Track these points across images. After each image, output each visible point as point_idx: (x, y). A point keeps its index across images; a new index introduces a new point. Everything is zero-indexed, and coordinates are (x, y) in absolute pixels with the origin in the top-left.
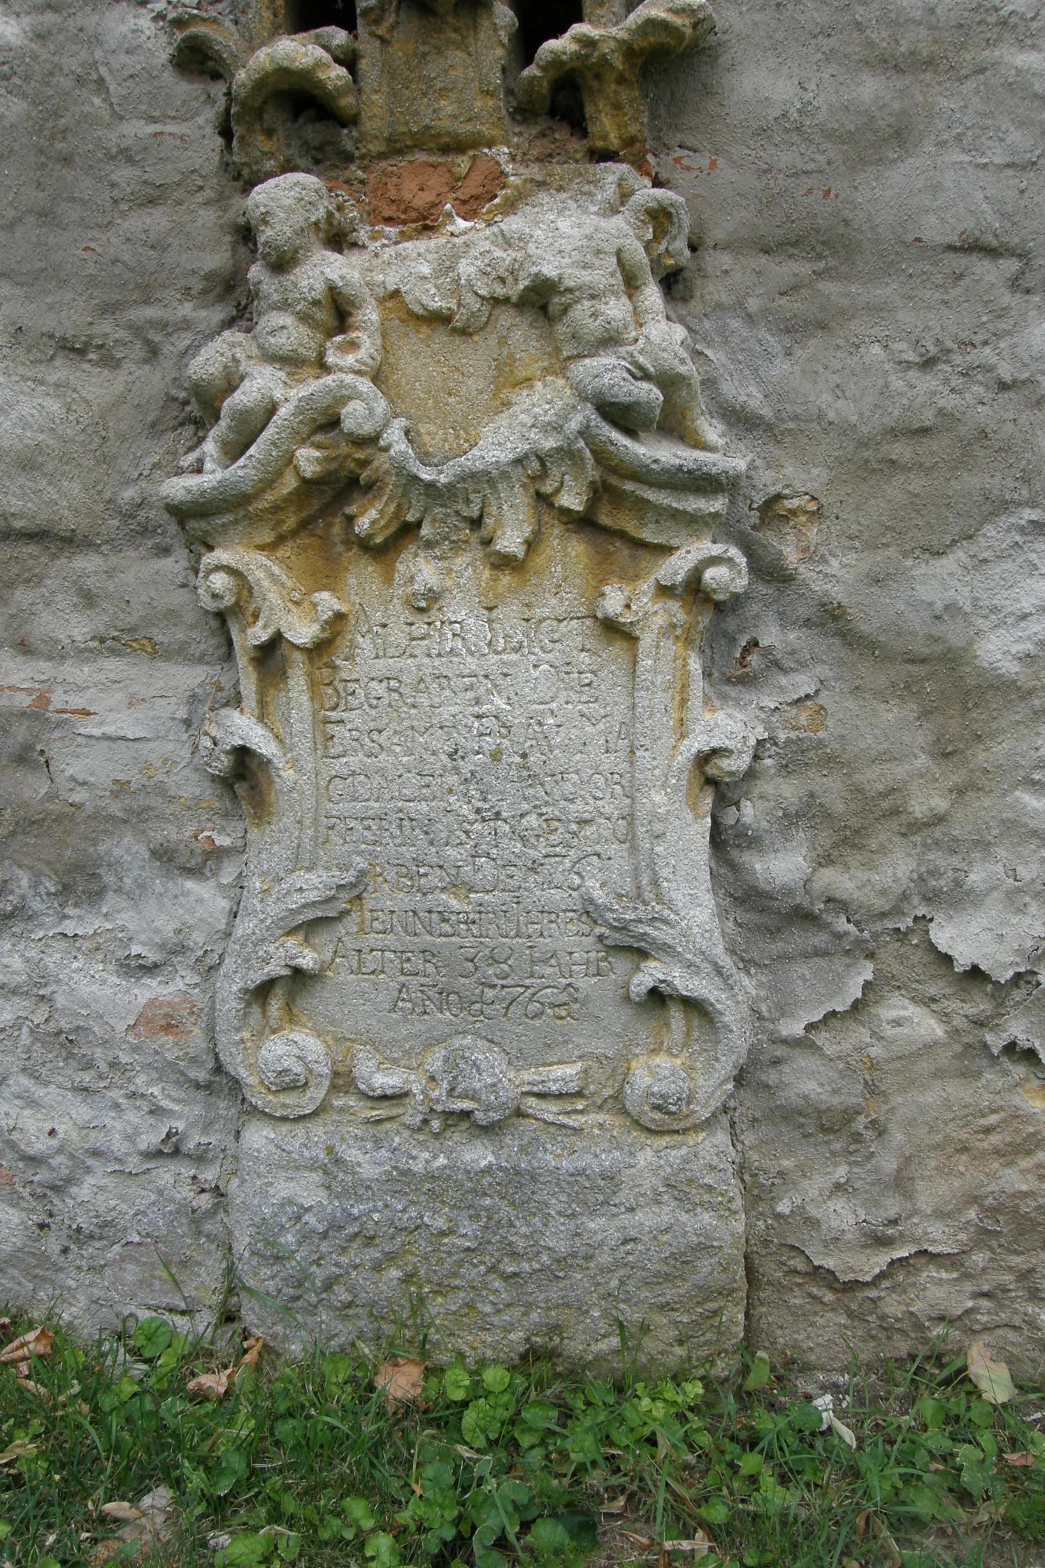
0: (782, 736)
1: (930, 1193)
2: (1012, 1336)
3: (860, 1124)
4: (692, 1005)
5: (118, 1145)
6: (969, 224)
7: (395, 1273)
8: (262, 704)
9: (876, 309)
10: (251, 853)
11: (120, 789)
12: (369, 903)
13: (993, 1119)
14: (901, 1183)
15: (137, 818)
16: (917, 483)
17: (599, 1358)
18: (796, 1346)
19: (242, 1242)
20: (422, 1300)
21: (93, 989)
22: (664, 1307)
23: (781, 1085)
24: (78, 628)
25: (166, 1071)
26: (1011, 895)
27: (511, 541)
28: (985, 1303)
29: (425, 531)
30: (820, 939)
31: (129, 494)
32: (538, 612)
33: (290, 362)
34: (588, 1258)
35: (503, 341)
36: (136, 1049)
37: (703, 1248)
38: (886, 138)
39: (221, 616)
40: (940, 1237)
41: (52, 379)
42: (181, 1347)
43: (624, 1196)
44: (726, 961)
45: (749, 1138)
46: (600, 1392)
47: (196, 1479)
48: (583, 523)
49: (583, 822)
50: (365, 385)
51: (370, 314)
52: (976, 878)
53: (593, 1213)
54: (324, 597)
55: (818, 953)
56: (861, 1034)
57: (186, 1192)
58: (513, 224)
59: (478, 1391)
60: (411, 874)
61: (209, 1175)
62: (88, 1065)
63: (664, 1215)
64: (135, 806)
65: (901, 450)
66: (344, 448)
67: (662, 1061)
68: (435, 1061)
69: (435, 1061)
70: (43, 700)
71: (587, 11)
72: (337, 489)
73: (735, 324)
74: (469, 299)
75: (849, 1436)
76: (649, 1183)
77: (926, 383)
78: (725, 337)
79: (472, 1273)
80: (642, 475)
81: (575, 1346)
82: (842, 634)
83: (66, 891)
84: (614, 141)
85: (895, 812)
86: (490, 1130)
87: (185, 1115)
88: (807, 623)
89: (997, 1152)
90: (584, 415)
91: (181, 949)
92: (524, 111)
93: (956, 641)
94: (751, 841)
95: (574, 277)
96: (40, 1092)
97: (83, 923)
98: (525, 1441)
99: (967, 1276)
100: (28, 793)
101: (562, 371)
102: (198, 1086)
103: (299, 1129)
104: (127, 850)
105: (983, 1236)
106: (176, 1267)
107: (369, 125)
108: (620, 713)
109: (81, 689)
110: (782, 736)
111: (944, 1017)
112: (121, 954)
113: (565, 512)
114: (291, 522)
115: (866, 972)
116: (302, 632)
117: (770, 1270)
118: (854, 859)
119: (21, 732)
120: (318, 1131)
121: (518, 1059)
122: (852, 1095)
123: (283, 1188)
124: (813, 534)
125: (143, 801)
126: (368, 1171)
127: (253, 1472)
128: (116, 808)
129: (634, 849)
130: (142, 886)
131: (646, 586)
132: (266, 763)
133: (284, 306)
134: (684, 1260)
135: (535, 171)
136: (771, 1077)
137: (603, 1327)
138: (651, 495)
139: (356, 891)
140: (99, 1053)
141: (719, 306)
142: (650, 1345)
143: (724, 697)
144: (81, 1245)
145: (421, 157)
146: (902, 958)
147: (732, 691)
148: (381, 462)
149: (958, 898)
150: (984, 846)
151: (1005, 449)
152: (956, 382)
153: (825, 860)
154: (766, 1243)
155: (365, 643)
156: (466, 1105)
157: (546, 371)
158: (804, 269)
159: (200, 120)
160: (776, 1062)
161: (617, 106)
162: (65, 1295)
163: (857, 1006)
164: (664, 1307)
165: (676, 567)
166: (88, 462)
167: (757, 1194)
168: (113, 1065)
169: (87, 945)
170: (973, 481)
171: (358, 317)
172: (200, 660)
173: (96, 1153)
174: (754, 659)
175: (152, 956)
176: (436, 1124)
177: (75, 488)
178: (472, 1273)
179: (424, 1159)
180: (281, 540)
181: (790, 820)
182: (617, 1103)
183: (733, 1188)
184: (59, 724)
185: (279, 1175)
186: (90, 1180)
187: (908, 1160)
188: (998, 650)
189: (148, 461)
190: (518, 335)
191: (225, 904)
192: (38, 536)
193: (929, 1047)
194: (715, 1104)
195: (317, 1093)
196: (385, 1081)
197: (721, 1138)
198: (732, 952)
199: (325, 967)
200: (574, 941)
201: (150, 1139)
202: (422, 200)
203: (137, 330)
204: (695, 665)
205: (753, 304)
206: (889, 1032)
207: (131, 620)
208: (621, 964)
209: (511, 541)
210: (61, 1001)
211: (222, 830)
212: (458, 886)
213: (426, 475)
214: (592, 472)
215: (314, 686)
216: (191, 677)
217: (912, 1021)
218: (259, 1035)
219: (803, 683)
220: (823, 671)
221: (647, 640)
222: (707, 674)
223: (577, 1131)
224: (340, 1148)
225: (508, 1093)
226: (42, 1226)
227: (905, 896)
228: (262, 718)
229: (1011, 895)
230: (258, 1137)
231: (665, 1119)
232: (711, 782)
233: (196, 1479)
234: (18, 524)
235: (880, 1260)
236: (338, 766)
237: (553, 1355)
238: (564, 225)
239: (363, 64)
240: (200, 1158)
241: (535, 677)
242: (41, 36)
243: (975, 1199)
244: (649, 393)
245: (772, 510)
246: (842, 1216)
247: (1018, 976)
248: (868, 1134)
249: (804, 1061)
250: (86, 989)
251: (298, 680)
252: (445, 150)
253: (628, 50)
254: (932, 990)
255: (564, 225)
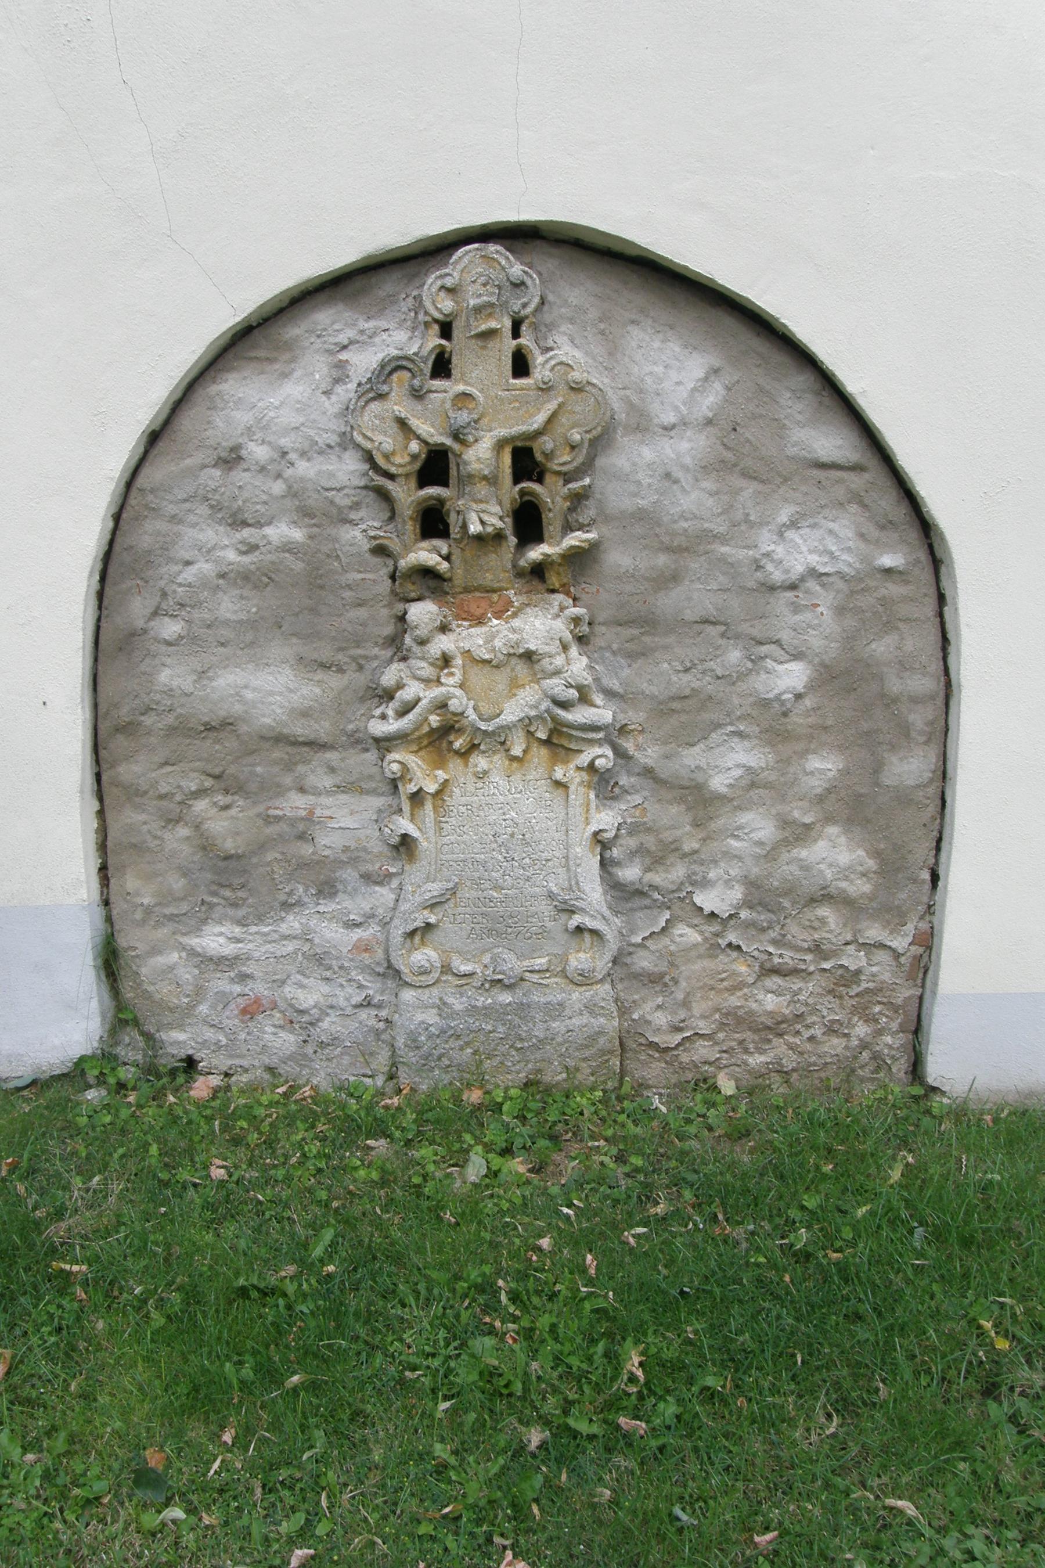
0: (629, 821)
1: (697, 1009)
2: (737, 1069)
3: (667, 979)
4: (594, 932)
5: (342, 1003)
6: (704, 613)
7: (469, 1050)
8: (412, 815)
9: (666, 647)
10: (405, 876)
11: (346, 849)
12: (458, 895)
13: (724, 975)
14: (686, 1004)
15: (354, 861)
16: (684, 718)
17: (558, 1083)
18: (643, 1077)
19: (400, 1042)
20: (481, 1061)
21: (332, 935)
22: (585, 1059)
23: (633, 963)
24: (328, 782)
25: (364, 969)
26: (727, 882)
27: (517, 751)
28: (725, 1055)
29: (482, 747)
30: (647, 902)
31: (351, 727)
32: (528, 777)
33: (426, 681)
34: (553, 1039)
35: (513, 670)
36: (351, 960)
37: (601, 1033)
38: (670, 579)
39: (394, 780)
40: (704, 1027)
41: (316, 678)
42: (371, 1091)
43: (568, 1012)
44: (607, 913)
45: (619, 987)
46: (559, 1097)
47: (397, 1134)
48: (547, 742)
49: (547, 860)
50: (458, 692)
51: (459, 661)
52: (712, 875)
53: (554, 1020)
54: (440, 772)
55: (646, 907)
56: (667, 941)
57: (372, 1022)
58: (516, 623)
59: (507, 1098)
60: (477, 883)
61: (384, 1013)
62: (329, 968)
63: (584, 1019)
64: (352, 856)
65: (675, 705)
66: (449, 716)
67: (582, 955)
68: (487, 959)
69: (487, 959)
70: (311, 812)
71: (546, 535)
72: (447, 730)
73: (607, 655)
74: (499, 655)
75: (664, 1109)
76: (578, 1006)
77: (686, 678)
78: (603, 660)
79: (503, 1049)
80: (571, 726)
81: (547, 1078)
82: (653, 779)
83: (320, 892)
84: (557, 586)
85: (677, 849)
86: (510, 987)
87: (373, 988)
88: (639, 774)
89: (727, 989)
90: (546, 704)
91: (373, 916)
92: (520, 574)
93: (701, 780)
94: (618, 864)
95: (543, 649)
96: (305, 981)
97: (328, 906)
98: (529, 1116)
99: (716, 1043)
100: (303, 852)
101: (538, 683)
102: (379, 974)
103: (427, 991)
104: (349, 875)
105: (722, 1026)
106: (368, 1055)
107: (456, 582)
108: (562, 816)
109: (329, 808)
110: (629, 821)
111: (701, 933)
112: (345, 919)
113: (540, 740)
114: (425, 742)
115: (667, 915)
116: (431, 788)
117: (631, 1044)
118: (661, 869)
119: (301, 827)
120: (435, 991)
121: (521, 957)
122: (663, 967)
123: (419, 1017)
124: (640, 739)
125: (356, 854)
126: (458, 1007)
127: (419, 1131)
128: (344, 857)
129: (568, 870)
130: (355, 890)
131: (572, 766)
132: (415, 840)
133: (423, 658)
134: (593, 1038)
135: (523, 599)
136: (628, 960)
137: (559, 1070)
138: (574, 733)
139: (454, 891)
140: (334, 962)
141: (601, 648)
142: (579, 1076)
143: (604, 805)
144: (322, 1048)
145: (478, 594)
146: (682, 909)
147: (608, 803)
148: (465, 722)
149: (705, 884)
150: (715, 862)
151: (720, 703)
152: (699, 676)
153: (648, 870)
154: (628, 1032)
155: (456, 790)
156: (500, 977)
157: (531, 681)
158: (636, 632)
159: (381, 573)
160: (630, 954)
161: (559, 574)
162: (314, 1072)
163: (663, 929)
164: (585, 1059)
165: (584, 759)
166: (333, 713)
167: (623, 1011)
168: (341, 967)
169: (328, 916)
170: (706, 716)
171: (454, 663)
172: (382, 794)
173: (332, 1007)
174: (617, 790)
175: (359, 920)
176: (487, 986)
177: (327, 724)
178: (503, 1049)
179: (481, 1001)
180: (420, 749)
181: (633, 854)
182: (563, 974)
183: (613, 1008)
184: (319, 823)
185: (418, 1011)
186: (328, 1019)
187: (688, 994)
188: (719, 783)
189: (359, 713)
190: (519, 667)
191: (393, 896)
192: (310, 744)
193: (695, 946)
194: (604, 972)
195: (435, 975)
196: (465, 968)
197: (607, 987)
198: (610, 908)
199: (439, 921)
200: (545, 908)
201: (357, 999)
202: (478, 612)
203: (354, 659)
204: (592, 796)
205: (615, 646)
206: (678, 939)
207: (352, 779)
208: (564, 916)
209: (517, 751)
210: (317, 941)
211: (392, 866)
212: (497, 888)
213: (483, 726)
214: (550, 725)
215: (435, 807)
216: (379, 802)
217: (687, 934)
218: (409, 951)
219: (637, 799)
220: (646, 793)
221: (572, 788)
222: (597, 796)
223: (547, 986)
224: (445, 998)
225: (518, 971)
226: (305, 1041)
227: (682, 883)
228: (412, 820)
229: (727, 882)
230: (408, 995)
231: (584, 979)
232: (599, 841)
233: (397, 1134)
234: (301, 739)
235: (678, 1038)
236: (446, 840)
237: (538, 1083)
238: (537, 623)
239: (453, 558)
240: (379, 1006)
241: (528, 802)
242: (311, 537)
243: (718, 1010)
244: (573, 693)
245: (623, 730)
246: (661, 1019)
247: (731, 916)
248: (671, 983)
249: (642, 953)
250: (329, 935)
251: (429, 806)
252: (488, 591)
253: (563, 556)
254: (696, 922)
255: (537, 623)
